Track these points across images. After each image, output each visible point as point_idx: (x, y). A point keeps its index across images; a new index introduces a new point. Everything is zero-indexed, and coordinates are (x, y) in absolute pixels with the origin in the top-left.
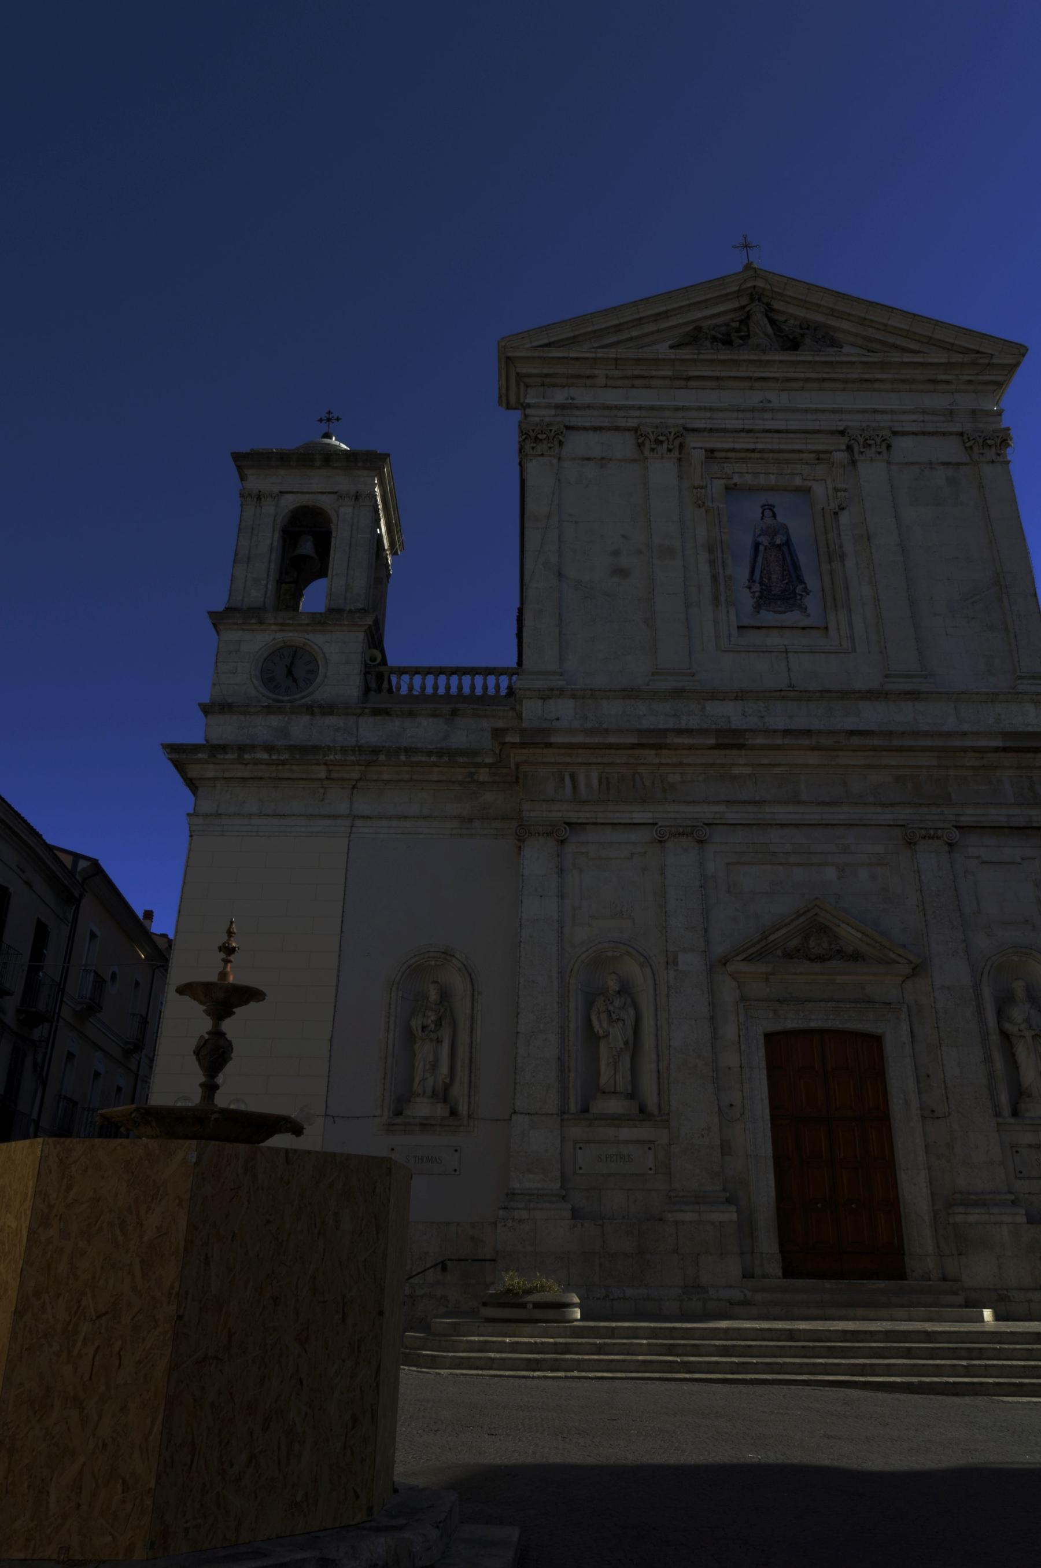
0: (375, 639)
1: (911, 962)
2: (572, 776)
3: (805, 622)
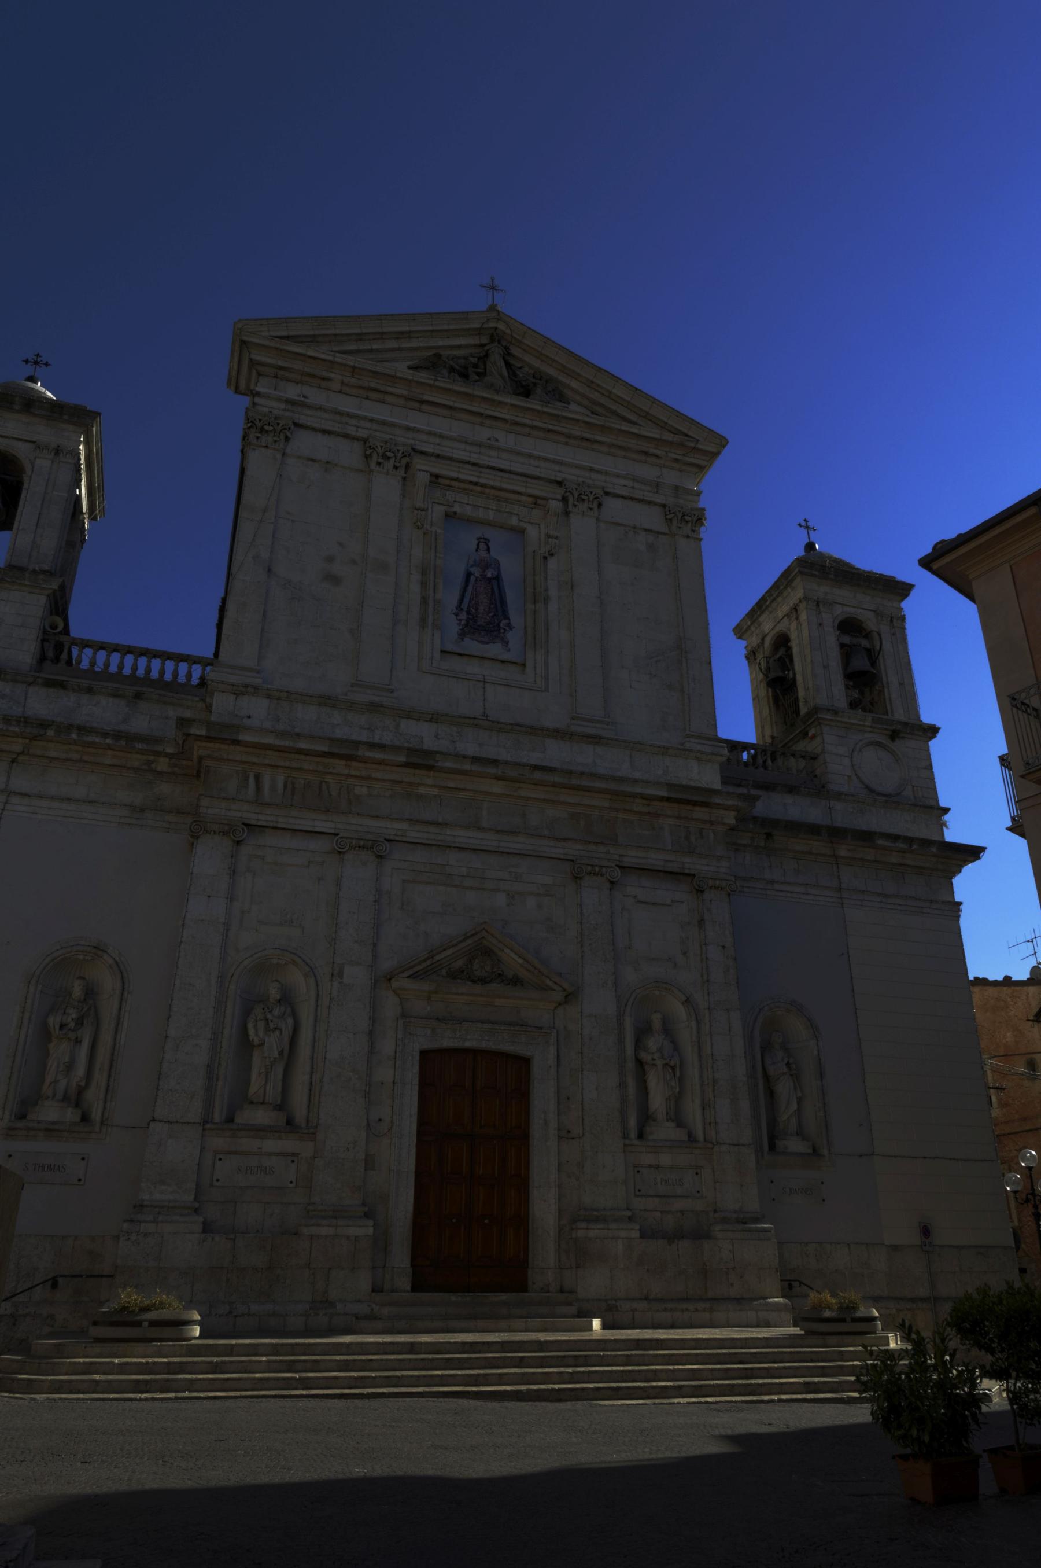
0: (59, 605)
1: (565, 990)
2: (257, 777)
3: (505, 656)
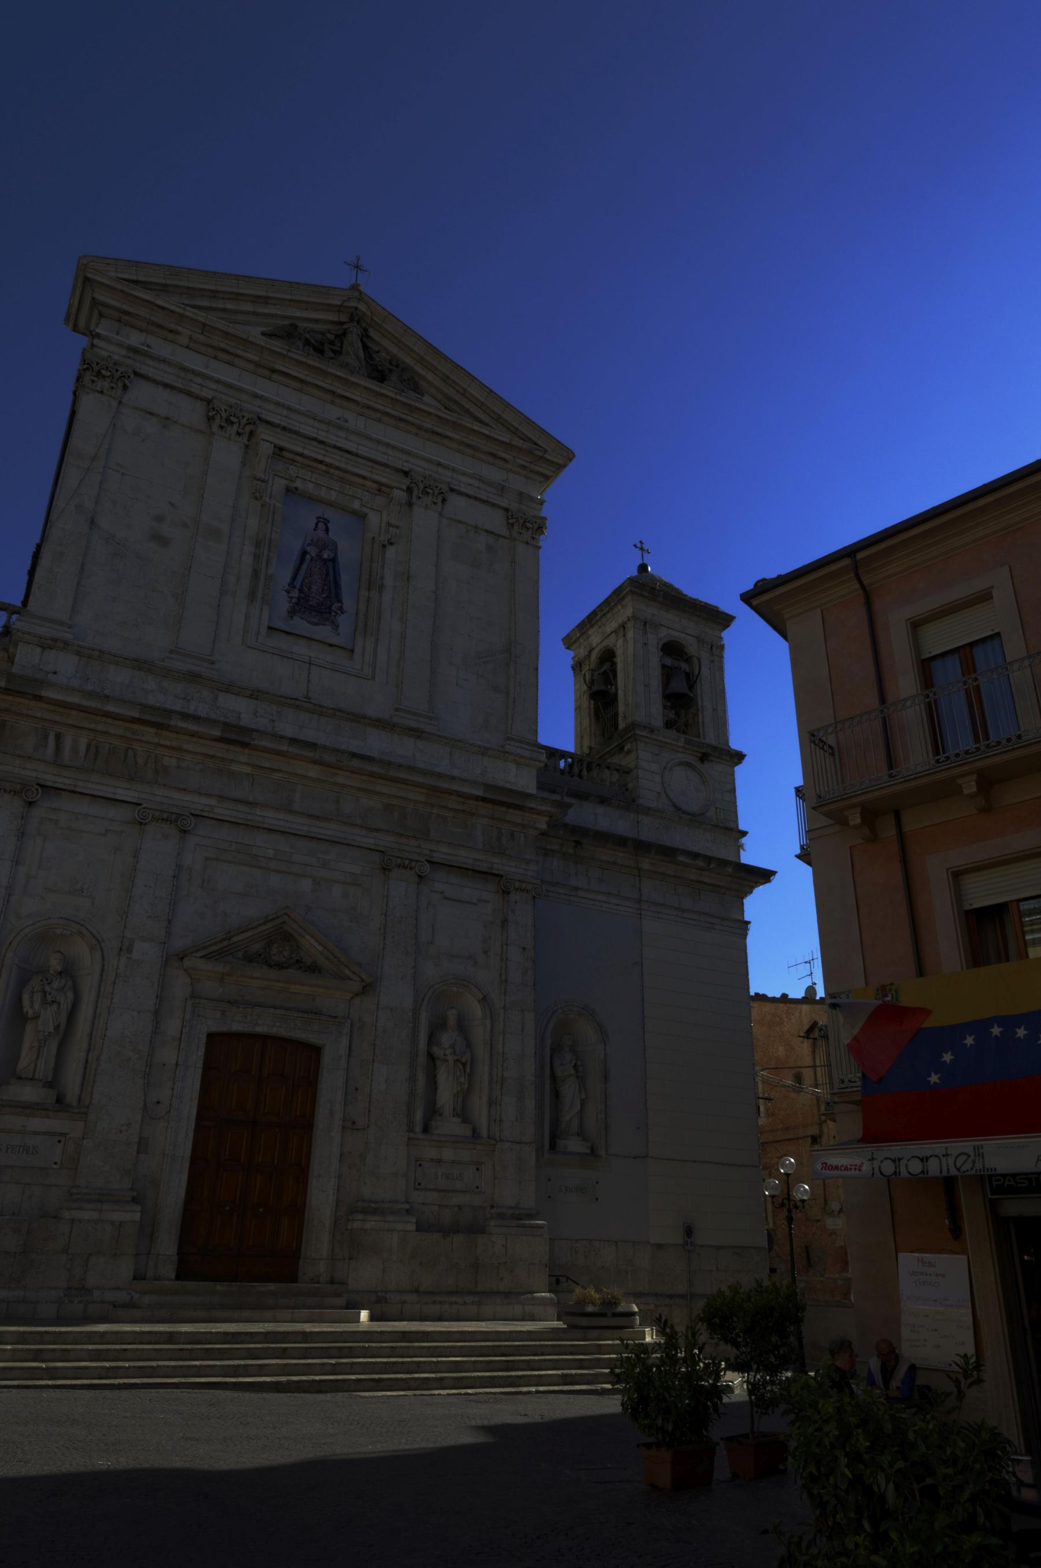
2: (58, 737)
3: (334, 640)
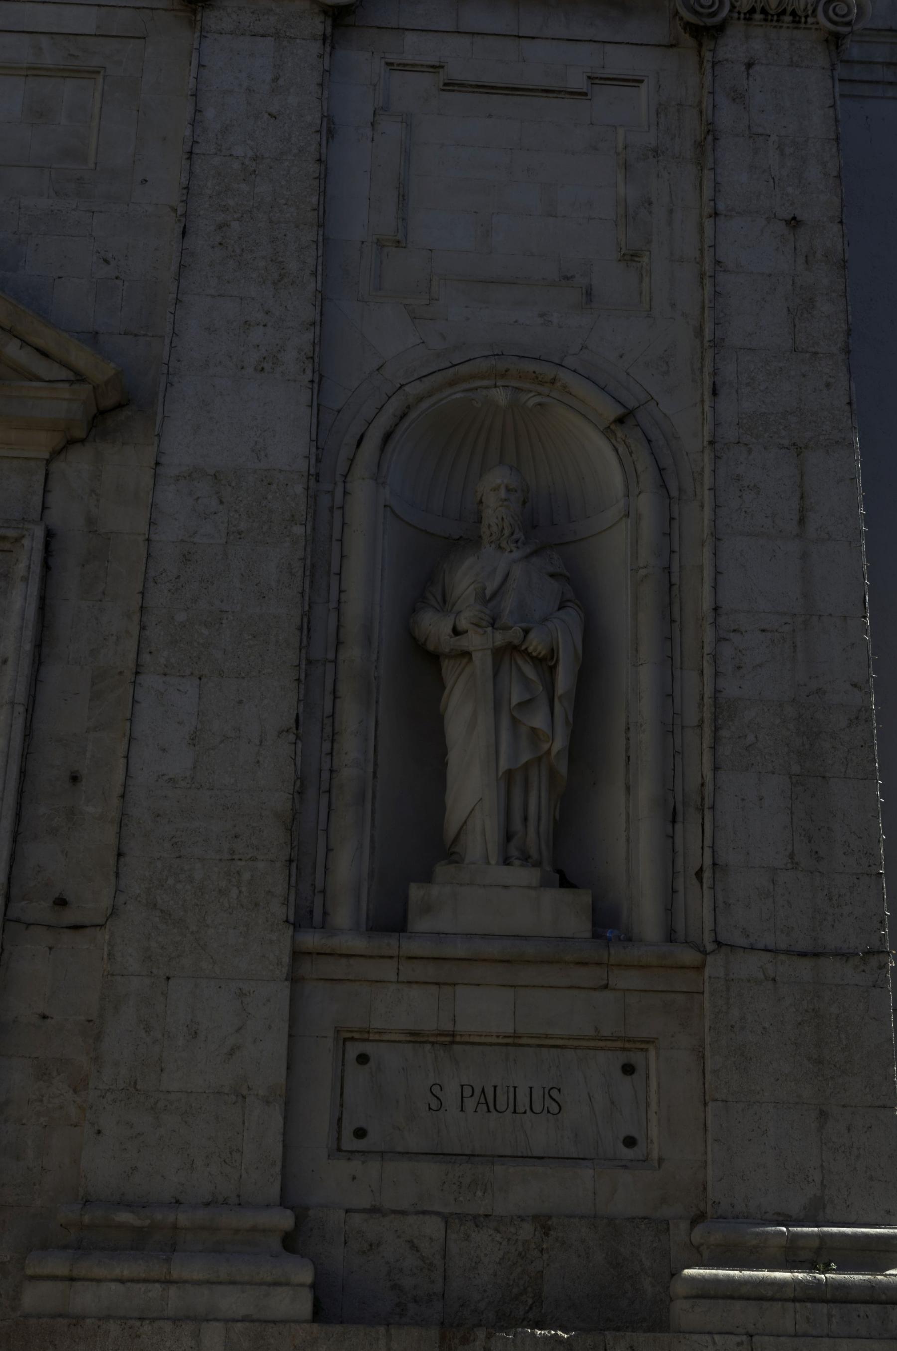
1: (79, 378)
